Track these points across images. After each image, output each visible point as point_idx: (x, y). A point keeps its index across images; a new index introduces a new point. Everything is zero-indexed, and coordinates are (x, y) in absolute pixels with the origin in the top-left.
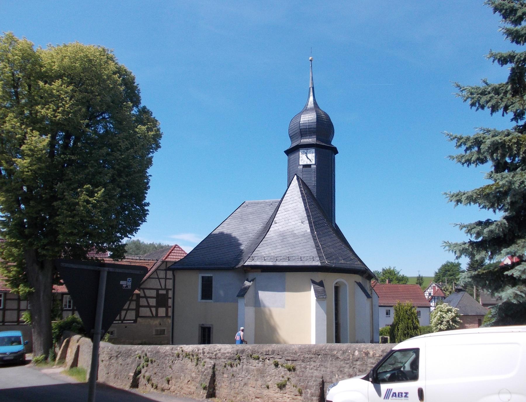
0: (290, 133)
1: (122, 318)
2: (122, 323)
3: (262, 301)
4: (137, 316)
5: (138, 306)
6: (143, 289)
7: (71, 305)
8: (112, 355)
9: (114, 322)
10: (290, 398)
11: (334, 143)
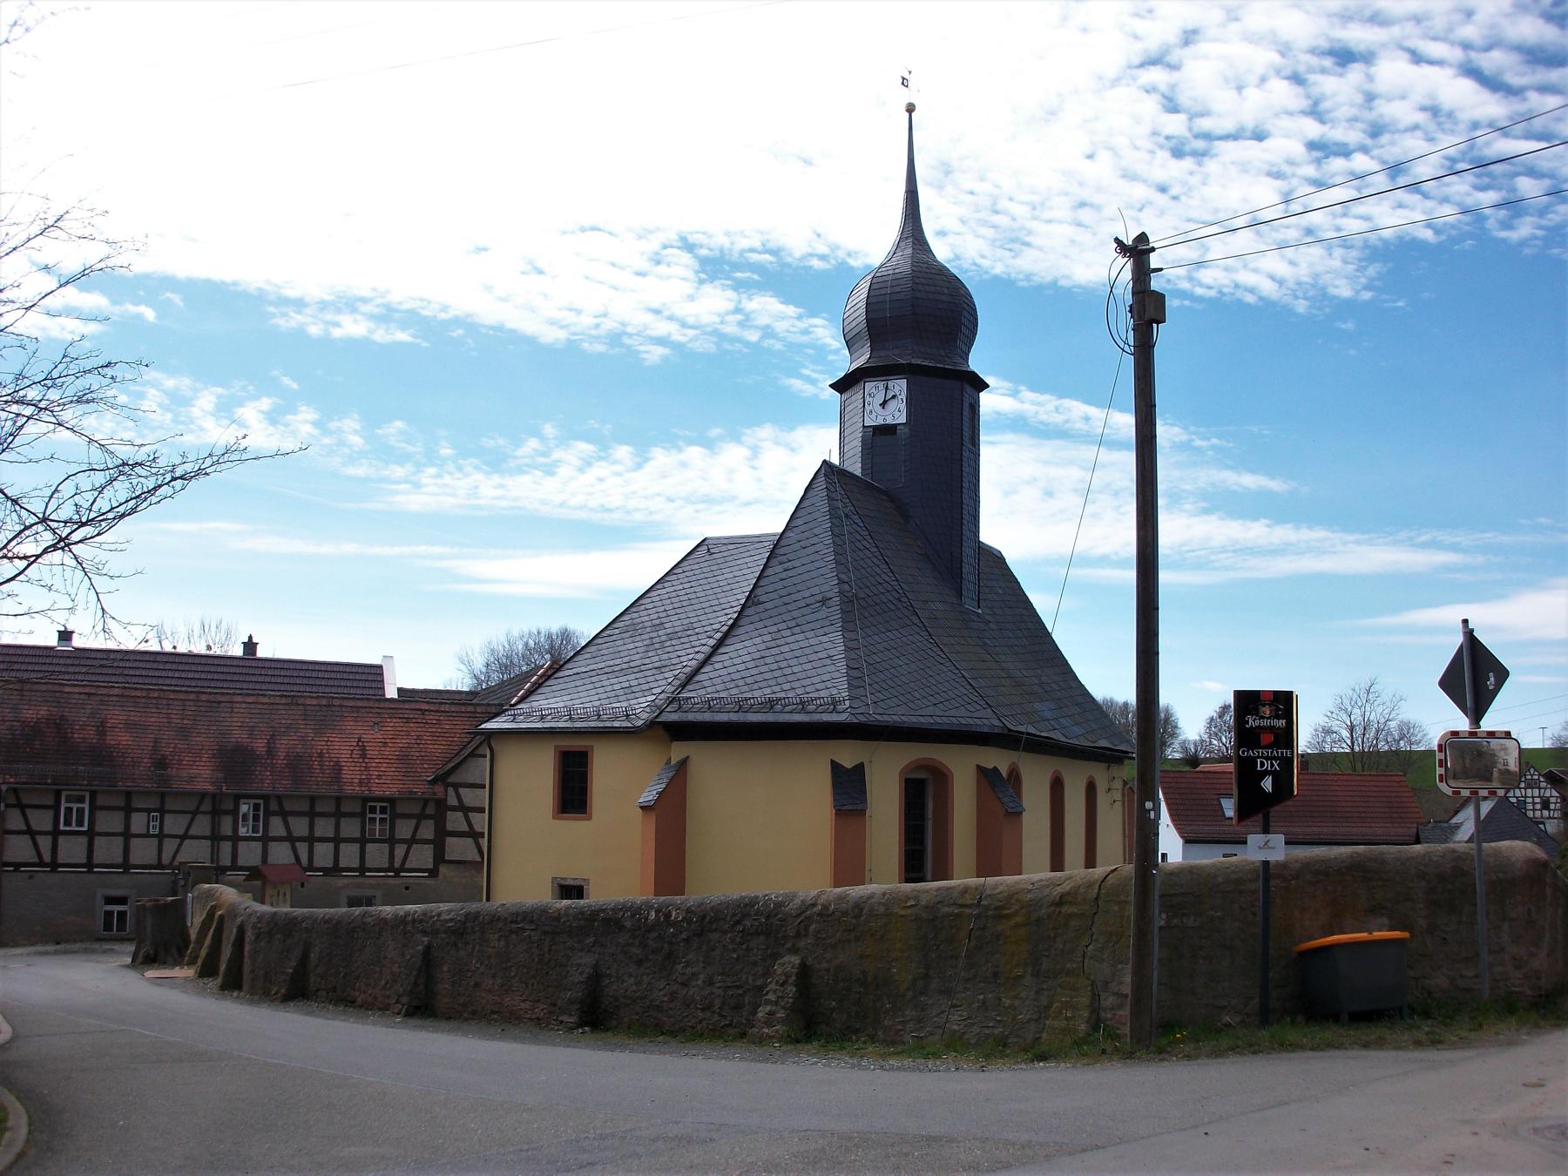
0: (874, 287)
1: (397, 865)
2: (397, 875)
3: (1511, 1043)
4: (439, 858)
5: (442, 834)
6: (456, 786)
7: (259, 815)
8: (262, 930)
9: (367, 874)
10: (545, 1011)
11: (977, 362)
